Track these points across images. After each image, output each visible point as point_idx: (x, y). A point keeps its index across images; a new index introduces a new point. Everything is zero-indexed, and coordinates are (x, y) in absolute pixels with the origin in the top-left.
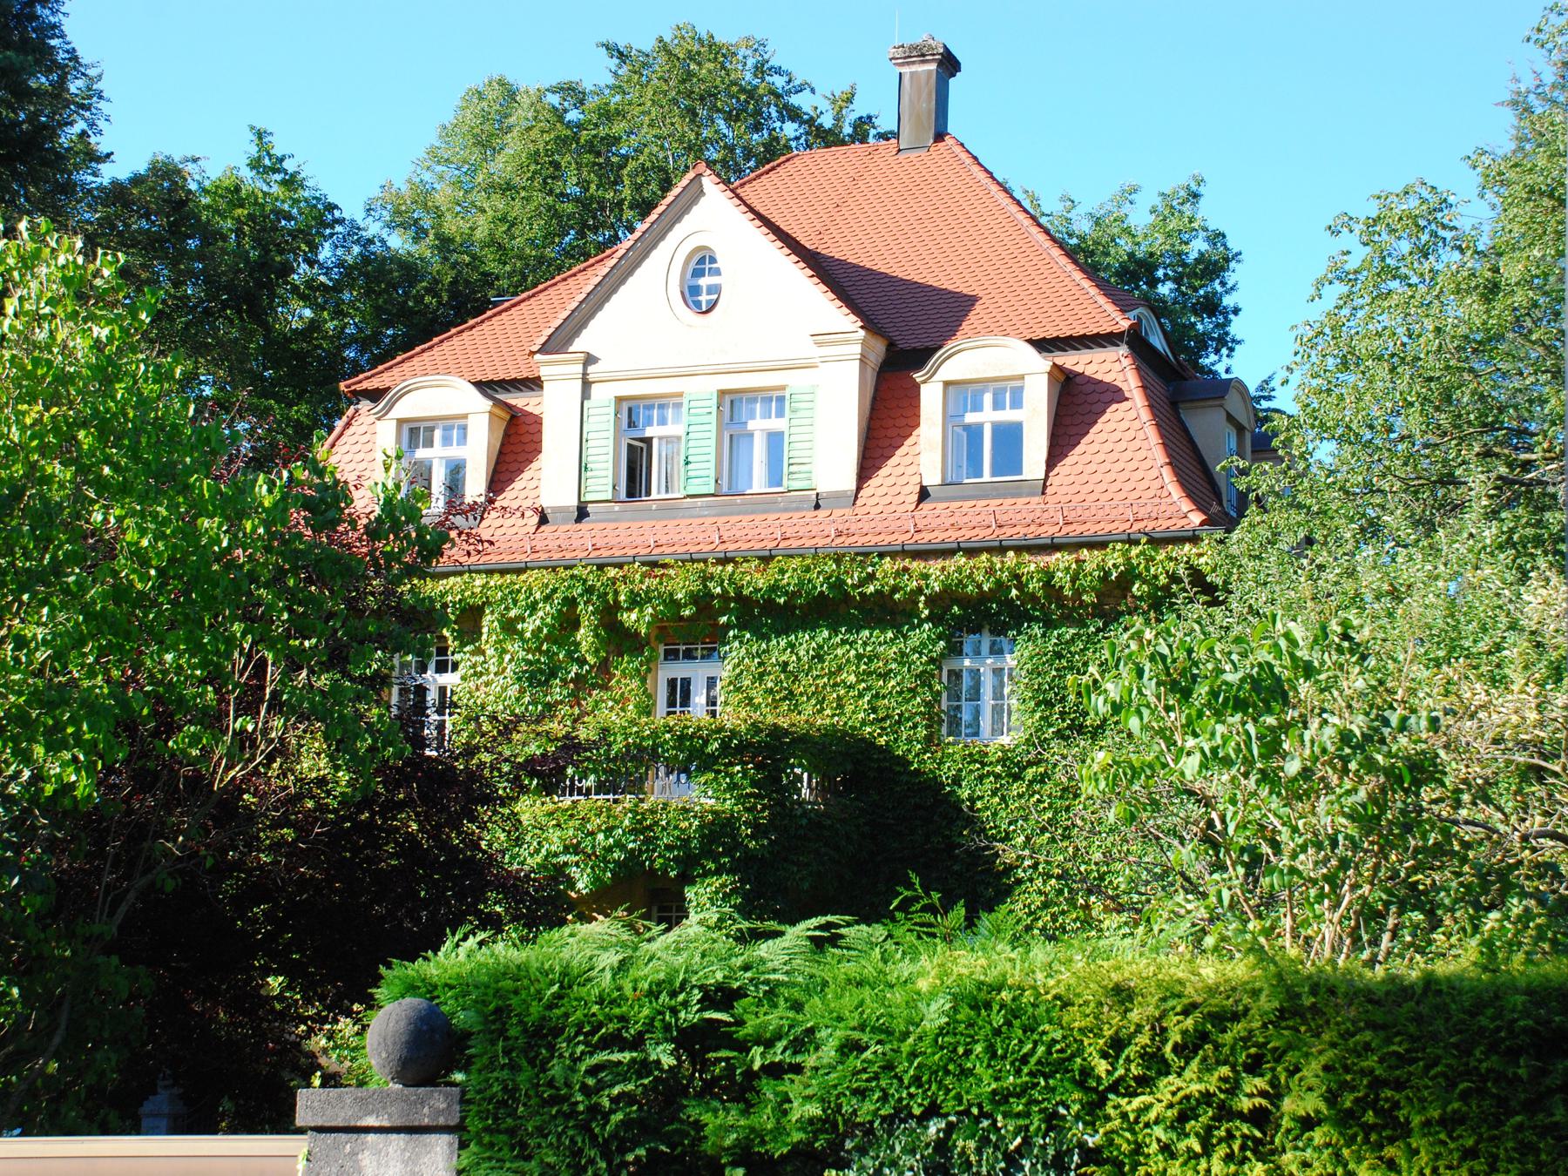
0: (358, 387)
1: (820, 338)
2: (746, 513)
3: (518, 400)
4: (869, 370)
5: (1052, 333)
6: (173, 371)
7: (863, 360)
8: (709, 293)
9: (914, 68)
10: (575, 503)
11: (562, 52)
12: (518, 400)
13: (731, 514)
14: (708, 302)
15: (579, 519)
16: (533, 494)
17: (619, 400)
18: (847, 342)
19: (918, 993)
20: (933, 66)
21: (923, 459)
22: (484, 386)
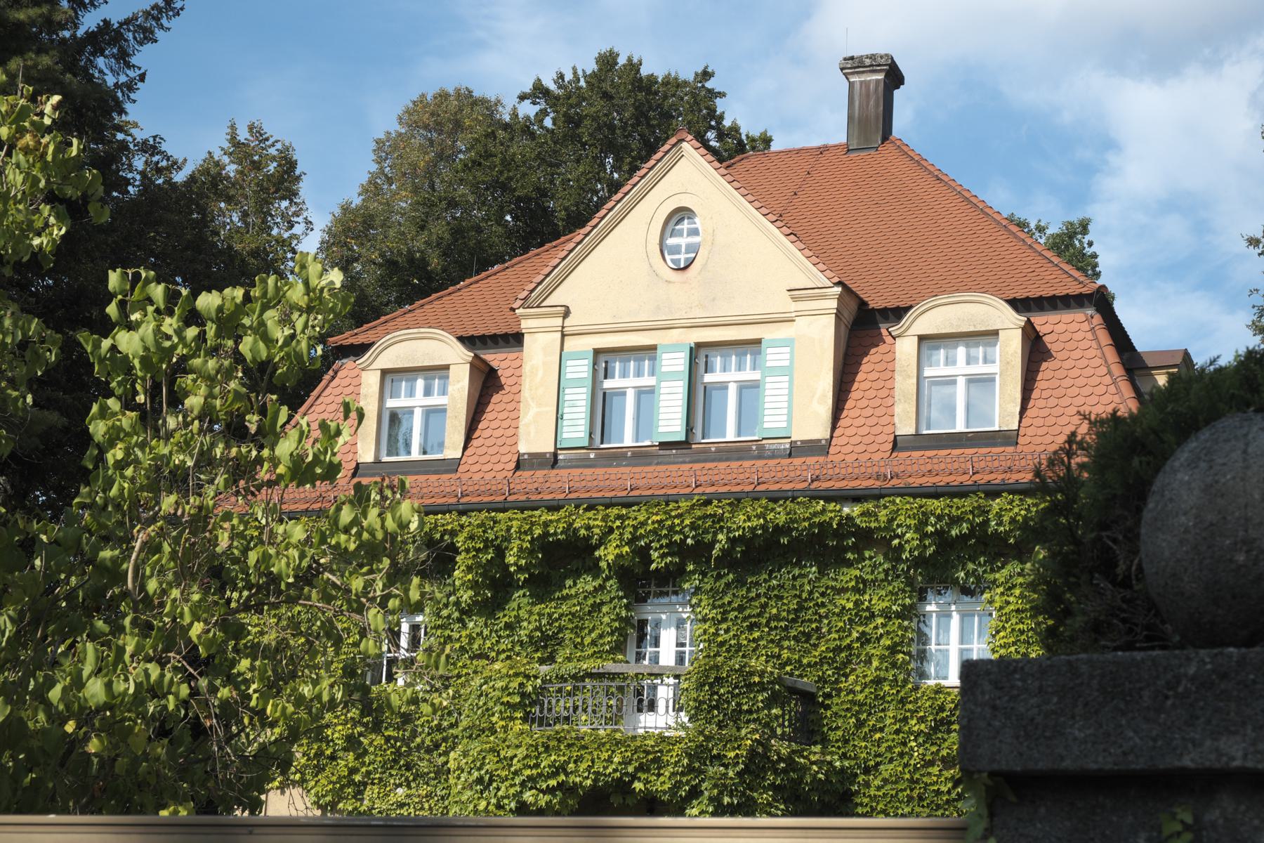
0: (345, 343)
1: (796, 293)
2: (720, 460)
3: (494, 358)
4: (843, 327)
5: (1034, 292)
6: (45, 534)
7: (838, 316)
8: (687, 252)
9: (863, 78)
10: (552, 450)
11: (517, 60)
12: (494, 358)
13: (705, 461)
14: (686, 259)
15: (553, 467)
16: (509, 441)
17: (597, 352)
18: (823, 297)
19: (1212, 524)
20: (881, 76)
21: (898, 409)
22: (467, 341)
